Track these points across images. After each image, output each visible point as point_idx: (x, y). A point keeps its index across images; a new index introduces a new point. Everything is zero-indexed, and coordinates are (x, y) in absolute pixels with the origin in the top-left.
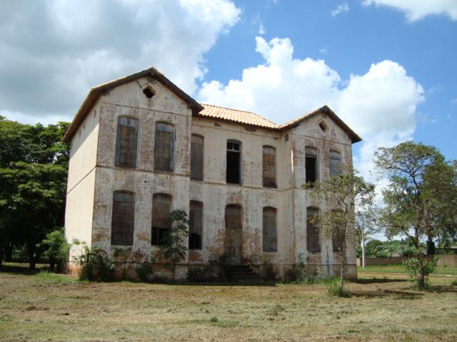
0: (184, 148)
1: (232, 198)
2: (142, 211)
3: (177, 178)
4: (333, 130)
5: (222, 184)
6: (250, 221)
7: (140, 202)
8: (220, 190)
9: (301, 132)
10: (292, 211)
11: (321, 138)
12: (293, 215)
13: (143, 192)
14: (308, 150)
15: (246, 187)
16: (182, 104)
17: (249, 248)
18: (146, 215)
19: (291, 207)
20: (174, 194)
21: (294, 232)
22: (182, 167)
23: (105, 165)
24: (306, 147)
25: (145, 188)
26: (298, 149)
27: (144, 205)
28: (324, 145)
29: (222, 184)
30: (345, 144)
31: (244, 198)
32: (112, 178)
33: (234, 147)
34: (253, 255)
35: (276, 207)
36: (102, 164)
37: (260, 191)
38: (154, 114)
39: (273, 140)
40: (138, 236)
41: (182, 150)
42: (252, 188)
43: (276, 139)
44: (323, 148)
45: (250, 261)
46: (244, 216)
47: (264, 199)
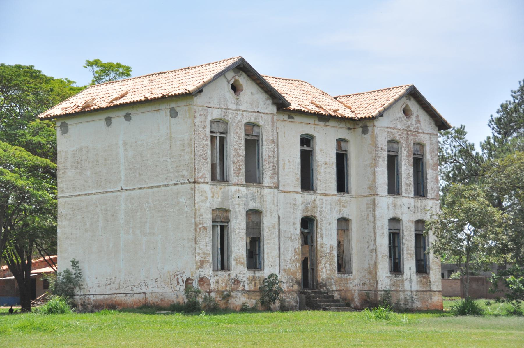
0: (270, 154)
1: (306, 209)
2: (237, 231)
3: (266, 191)
4: (418, 116)
5: (297, 193)
6: (324, 236)
7: (235, 221)
8: (295, 200)
9: (381, 123)
10: (372, 224)
11: (404, 128)
12: (375, 228)
13: (237, 210)
14: (391, 145)
15: (321, 194)
16: (267, 99)
17: (324, 270)
18: (241, 236)
19: (371, 218)
20: (264, 210)
21: (376, 250)
22: (270, 177)
23: (202, 180)
24: (389, 142)
25: (239, 204)
26: (380, 146)
27: (239, 224)
28: (408, 138)
29: (297, 193)
30: (431, 134)
31: (319, 209)
32: (210, 195)
33: (306, 141)
34: (328, 279)
35: (350, 218)
36: (200, 180)
37: (334, 197)
38: (243, 115)
39: (346, 131)
40: (236, 260)
41: (269, 156)
42: (326, 195)
43: (349, 129)
44: (407, 142)
45: (325, 285)
46: (319, 230)
47: (337, 208)
